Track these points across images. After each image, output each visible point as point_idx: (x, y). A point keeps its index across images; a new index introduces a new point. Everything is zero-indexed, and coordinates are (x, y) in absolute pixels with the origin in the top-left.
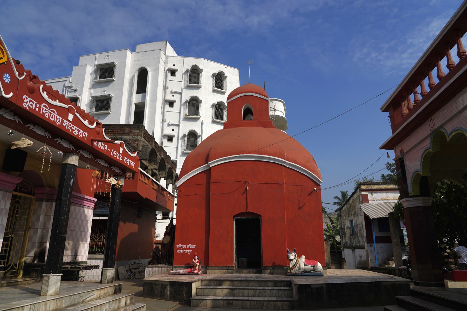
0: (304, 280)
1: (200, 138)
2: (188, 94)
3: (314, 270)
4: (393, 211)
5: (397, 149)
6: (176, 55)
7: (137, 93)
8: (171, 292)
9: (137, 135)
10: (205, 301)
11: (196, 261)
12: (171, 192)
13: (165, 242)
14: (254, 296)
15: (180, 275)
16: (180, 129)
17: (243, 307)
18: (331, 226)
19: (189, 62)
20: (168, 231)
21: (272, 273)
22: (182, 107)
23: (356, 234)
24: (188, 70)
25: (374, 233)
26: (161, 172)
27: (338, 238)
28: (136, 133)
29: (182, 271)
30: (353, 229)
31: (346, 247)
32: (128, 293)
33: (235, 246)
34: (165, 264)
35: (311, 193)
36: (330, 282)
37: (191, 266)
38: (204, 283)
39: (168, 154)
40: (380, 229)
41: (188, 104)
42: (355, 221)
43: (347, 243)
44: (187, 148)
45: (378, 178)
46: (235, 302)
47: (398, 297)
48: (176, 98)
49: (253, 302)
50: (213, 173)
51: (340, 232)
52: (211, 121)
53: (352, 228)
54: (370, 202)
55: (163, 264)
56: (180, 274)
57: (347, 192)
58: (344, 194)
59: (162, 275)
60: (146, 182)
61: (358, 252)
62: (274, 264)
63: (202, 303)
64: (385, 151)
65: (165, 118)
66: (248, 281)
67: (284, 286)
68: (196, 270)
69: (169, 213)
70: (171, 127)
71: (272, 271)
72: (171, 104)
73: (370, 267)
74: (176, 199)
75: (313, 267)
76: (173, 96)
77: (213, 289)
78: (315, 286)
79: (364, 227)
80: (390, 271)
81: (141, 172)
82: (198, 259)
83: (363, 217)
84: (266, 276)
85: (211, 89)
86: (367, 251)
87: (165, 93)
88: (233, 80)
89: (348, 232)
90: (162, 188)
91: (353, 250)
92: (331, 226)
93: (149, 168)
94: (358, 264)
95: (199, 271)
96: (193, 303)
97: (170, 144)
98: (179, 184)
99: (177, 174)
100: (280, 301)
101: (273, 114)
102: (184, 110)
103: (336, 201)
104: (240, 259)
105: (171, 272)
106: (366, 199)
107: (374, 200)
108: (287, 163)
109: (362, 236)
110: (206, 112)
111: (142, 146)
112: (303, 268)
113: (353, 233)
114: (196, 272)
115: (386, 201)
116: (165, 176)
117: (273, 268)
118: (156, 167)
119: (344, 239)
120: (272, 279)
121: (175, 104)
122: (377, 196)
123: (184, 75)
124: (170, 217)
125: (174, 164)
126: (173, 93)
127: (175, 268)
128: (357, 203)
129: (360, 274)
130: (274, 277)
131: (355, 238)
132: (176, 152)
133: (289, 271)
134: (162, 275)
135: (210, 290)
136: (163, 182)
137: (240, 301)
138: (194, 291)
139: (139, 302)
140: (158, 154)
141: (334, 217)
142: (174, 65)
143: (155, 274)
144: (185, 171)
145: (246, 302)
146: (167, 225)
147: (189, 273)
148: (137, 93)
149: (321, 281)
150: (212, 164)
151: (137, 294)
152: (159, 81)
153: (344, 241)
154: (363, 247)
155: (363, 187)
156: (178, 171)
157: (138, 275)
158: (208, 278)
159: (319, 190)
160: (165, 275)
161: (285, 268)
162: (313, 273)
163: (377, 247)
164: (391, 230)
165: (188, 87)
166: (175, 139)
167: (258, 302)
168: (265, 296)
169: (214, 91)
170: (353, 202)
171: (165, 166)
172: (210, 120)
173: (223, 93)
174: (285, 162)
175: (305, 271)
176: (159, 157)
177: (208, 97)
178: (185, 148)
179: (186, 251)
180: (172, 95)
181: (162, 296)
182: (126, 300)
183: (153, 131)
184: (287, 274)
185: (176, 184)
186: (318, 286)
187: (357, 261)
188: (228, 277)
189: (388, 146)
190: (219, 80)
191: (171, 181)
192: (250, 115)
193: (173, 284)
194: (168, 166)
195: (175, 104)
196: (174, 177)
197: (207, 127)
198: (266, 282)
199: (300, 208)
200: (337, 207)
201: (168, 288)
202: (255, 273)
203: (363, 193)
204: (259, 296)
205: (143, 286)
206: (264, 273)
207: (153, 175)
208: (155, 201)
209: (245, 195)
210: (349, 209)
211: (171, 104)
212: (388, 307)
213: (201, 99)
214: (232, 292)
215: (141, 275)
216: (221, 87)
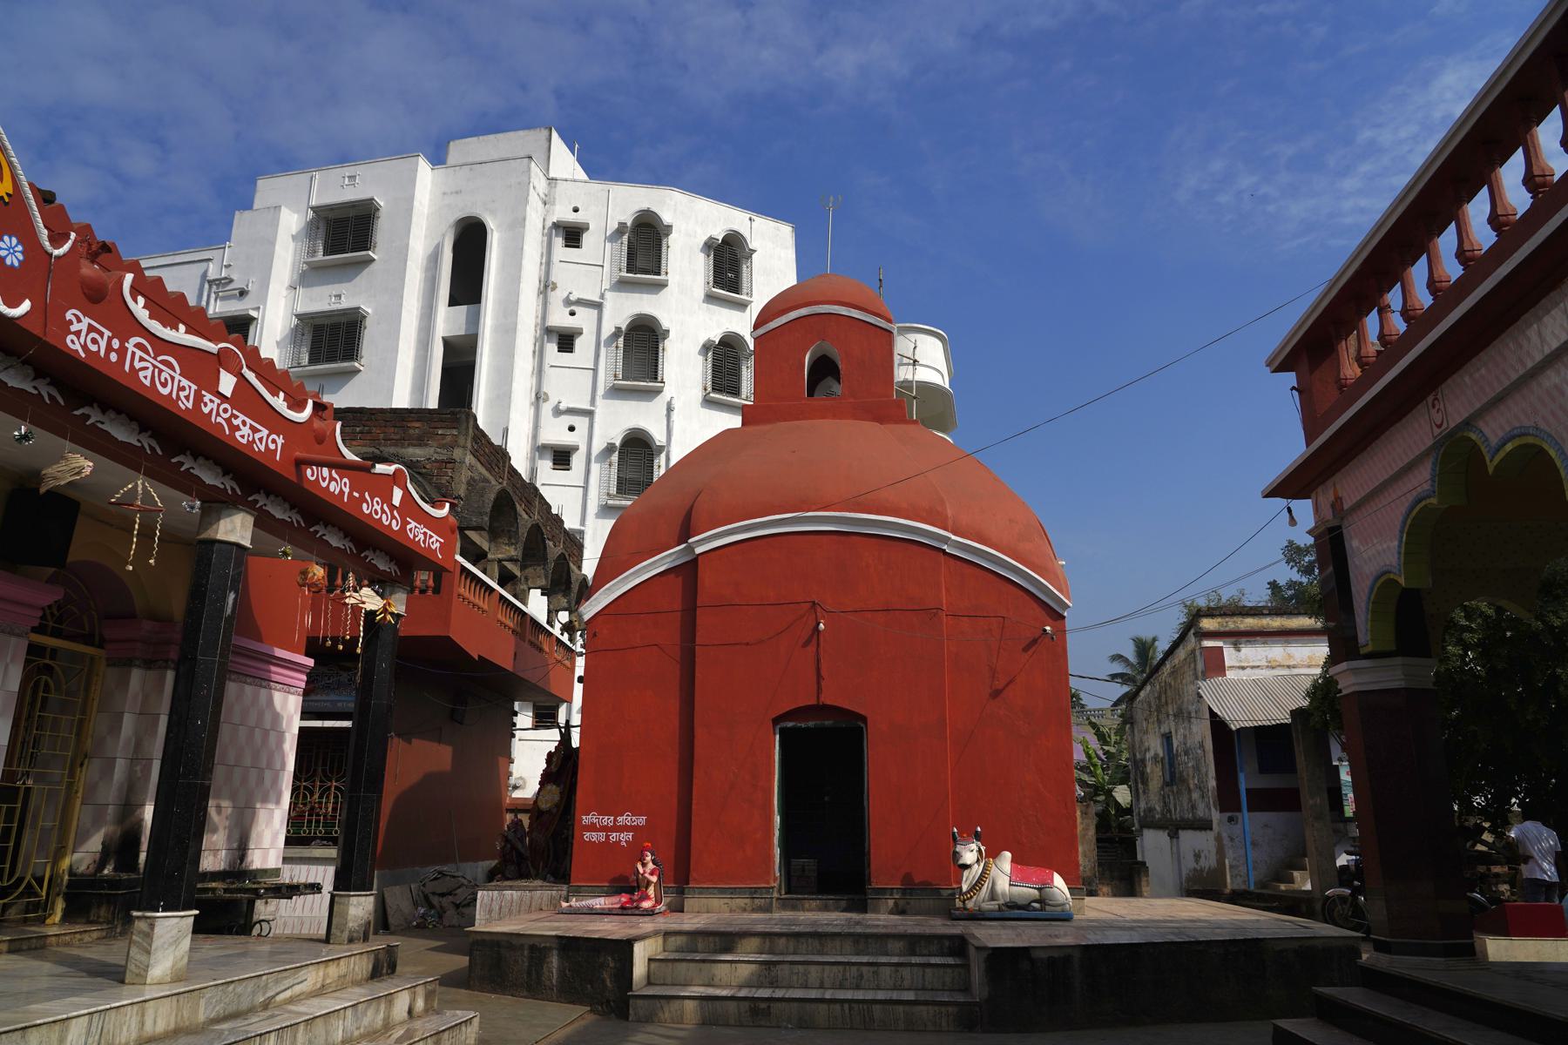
0: (1009, 932)
1: (663, 456)
2: (622, 310)
4: (1305, 703)
5: (1321, 499)
10: (676, 1004)
11: (647, 868)
13: (544, 806)
14: (841, 987)
15: (592, 915)
17: (804, 1024)
18: (1100, 753)
19: (627, 200)
21: (901, 911)
22: (603, 350)
23: (1184, 781)
24: (622, 225)
25: (1242, 777)
26: (530, 571)
27: (1122, 794)
28: (449, 439)
29: (599, 903)
30: (1172, 765)
31: (1150, 823)
33: (777, 819)
34: (544, 879)
35: (1035, 641)
36: (1094, 939)
37: (629, 886)
38: (675, 941)
39: (554, 511)
40: (1258, 761)
41: (621, 340)
43: (1151, 810)
44: (619, 490)
45: (1258, 595)
46: (776, 1007)
48: (584, 320)
49: (838, 1007)
50: (706, 577)
51: (1128, 773)
53: (1170, 759)
54: (1230, 674)
55: (536, 877)
56: (591, 912)
57: (1154, 640)
58: (1143, 648)
59: (534, 917)
61: (1190, 840)
62: (907, 878)
63: (666, 1009)
64: (1280, 502)
65: (545, 389)
66: (820, 937)
67: (942, 955)
69: (556, 708)
71: (901, 903)
72: (566, 341)
74: (580, 663)
75: (1040, 889)
76: (572, 314)
77: (704, 961)
78: (1043, 955)
80: (1293, 905)
81: (463, 569)
82: (654, 862)
84: (881, 919)
86: (1219, 839)
88: (775, 262)
89: (1155, 774)
90: (535, 623)
91: (1174, 836)
92: (1100, 753)
93: (490, 556)
95: (658, 902)
96: (637, 1008)
97: (561, 476)
98: (590, 609)
99: (585, 578)
100: (926, 1003)
101: (910, 377)
102: (611, 363)
103: (1118, 668)
104: (794, 861)
105: (565, 905)
106: (1216, 665)
107: (1243, 668)
108: (954, 542)
109: (1201, 788)
110: (683, 368)
111: (468, 483)
112: (1004, 894)
113: (1174, 779)
114: (646, 904)
115: (1285, 672)
116: (543, 582)
120: (901, 930)
121: (579, 343)
122: (1253, 653)
123: (608, 245)
124: (562, 720)
125: (574, 543)
126: (573, 304)
127: (577, 892)
128: (1189, 677)
131: (1179, 792)
132: (580, 503)
133: (959, 904)
134: (534, 917)
136: (537, 605)
138: (639, 969)
139: (455, 1004)
141: (1110, 723)
142: (576, 210)
144: (610, 566)
145: (814, 1006)
146: (552, 747)
147: (622, 908)
149: (1064, 937)
150: (704, 542)
151: (450, 981)
153: (1143, 805)
154: (1205, 825)
155: (1207, 624)
156: (589, 568)
157: (451, 916)
158: (687, 927)
159: (1061, 632)
160: (543, 915)
161: (945, 893)
162: (1039, 911)
163: (1251, 822)
165: (622, 285)
166: (577, 461)
168: (878, 988)
169: (710, 298)
170: (1174, 672)
171: (544, 550)
172: (697, 394)
173: (742, 306)
174: (946, 540)
175: (1012, 905)
176: (525, 519)
177: (691, 318)
178: (613, 490)
179: (614, 836)
181: (533, 987)
183: (506, 431)
184: (951, 915)
185: (581, 609)
186: (1056, 954)
188: (755, 922)
189: (1290, 486)
190: (728, 261)
192: (830, 381)
193: (569, 945)
194: (554, 550)
195: (578, 343)
196: (575, 587)
197: (687, 419)
198: (879, 940)
199: (996, 694)
200: (1120, 690)
201: (554, 961)
203: (1208, 643)
204: (858, 988)
205: (470, 953)
206: (876, 911)
207: (506, 579)
209: (811, 649)
210: (1159, 698)
211: (566, 341)
213: (665, 324)
214: (768, 972)
215: (462, 915)
216: (735, 286)
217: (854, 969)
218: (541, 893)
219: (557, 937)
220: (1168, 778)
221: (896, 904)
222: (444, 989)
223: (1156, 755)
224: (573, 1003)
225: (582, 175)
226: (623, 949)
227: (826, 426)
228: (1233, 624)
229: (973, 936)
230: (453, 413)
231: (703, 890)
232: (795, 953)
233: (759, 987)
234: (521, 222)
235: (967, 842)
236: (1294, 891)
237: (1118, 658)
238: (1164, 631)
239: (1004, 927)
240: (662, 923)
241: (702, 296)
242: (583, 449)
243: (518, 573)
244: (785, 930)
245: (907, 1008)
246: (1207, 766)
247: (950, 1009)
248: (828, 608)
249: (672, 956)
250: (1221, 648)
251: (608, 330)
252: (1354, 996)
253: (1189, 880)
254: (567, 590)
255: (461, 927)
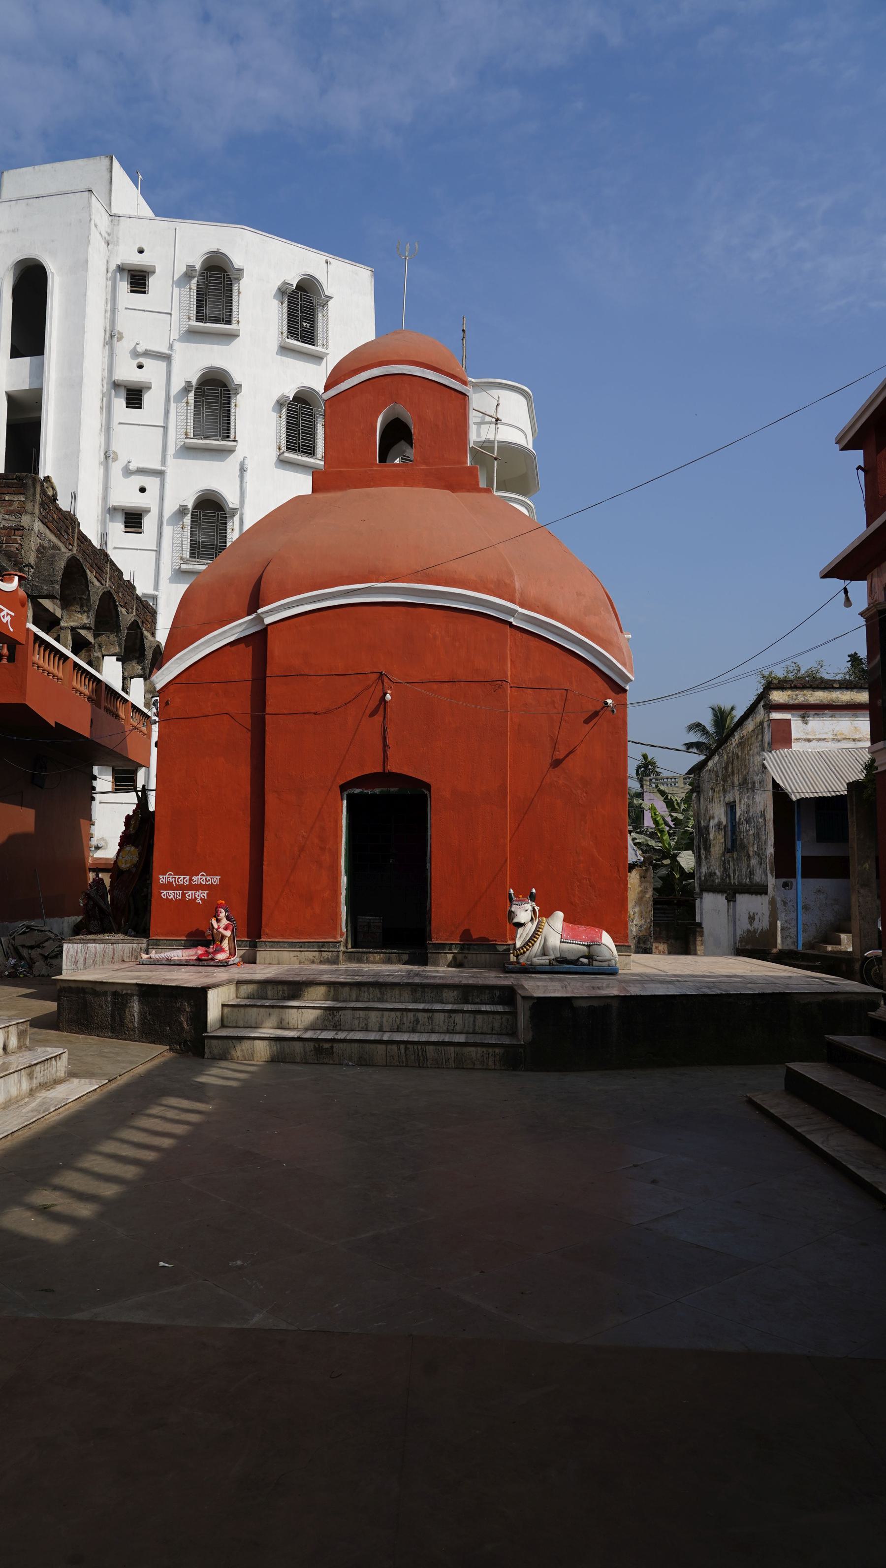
0: (556, 984)
1: (236, 518)
2: (194, 361)
3: (590, 957)
4: (861, 776)
5: (875, 580)
6: (147, 212)
7: (12, 357)
8: (140, 1013)
9: (20, 512)
10: (246, 1044)
11: (221, 924)
12: (141, 706)
13: (123, 866)
14: (399, 1030)
15: (171, 966)
16: (167, 486)
17: (364, 1062)
18: (669, 819)
19: (196, 240)
21: (457, 963)
22: (173, 406)
23: (744, 848)
24: (190, 270)
25: (799, 845)
26: (103, 638)
27: (687, 860)
28: (16, 505)
29: (178, 955)
30: (734, 832)
31: (710, 887)
32: (10, 1018)
33: (344, 879)
34: (126, 934)
35: (596, 714)
36: (635, 991)
37: (202, 939)
38: (246, 989)
39: (126, 577)
40: (818, 831)
41: (191, 395)
42: (743, 807)
43: (711, 875)
44: (192, 554)
46: (338, 1047)
47: (831, 1037)
48: (152, 374)
49: (395, 1047)
51: (692, 839)
52: (274, 459)
53: (733, 828)
54: (795, 746)
55: (117, 932)
56: (170, 963)
57: (732, 709)
58: (720, 716)
59: (116, 967)
60: (55, 672)
61: (746, 903)
62: (466, 935)
63: (238, 1048)
64: (837, 584)
65: (114, 447)
66: (380, 987)
68: (223, 950)
69: (135, 772)
71: (459, 957)
72: (134, 397)
73: (775, 951)
74: (155, 728)
75: (588, 946)
76: (140, 367)
77: (272, 1007)
78: (584, 1004)
79: (771, 825)
81: (37, 637)
82: (228, 918)
83: (770, 795)
84: (440, 971)
86: (772, 902)
87: (111, 355)
88: (352, 317)
89: (717, 840)
90: (110, 690)
91: (731, 899)
92: (669, 819)
93: (63, 624)
95: (232, 954)
96: (212, 1047)
97: (133, 539)
98: (163, 677)
99: (158, 646)
100: (475, 1045)
101: (492, 438)
102: (182, 417)
103: (694, 737)
104: (361, 919)
105: (145, 956)
107: (809, 740)
108: (521, 615)
109: (760, 855)
110: (257, 424)
111: (38, 550)
112: (554, 949)
113: (735, 845)
114: (221, 956)
115: (851, 745)
116: (117, 650)
117: (462, 947)
118: (85, 619)
119: (704, 863)
120: (456, 981)
122: (819, 726)
123: (176, 290)
124: (139, 786)
125: (147, 610)
126: (141, 356)
127: (156, 944)
128: (755, 750)
129: (733, 972)
131: (739, 858)
132: (153, 568)
133: (513, 958)
134: (116, 967)
135: (262, 1010)
136: (111, 671)
137: (356, 1045)
138: (213, 1013)
139: (45, 1043)
140: (91, 576)
141: (679, 793)
142: (141, 251)
144: (182, 636)
145: (373, 1046)
146: (130, 810)
147: (199, 959)
148: (12, 357)
149: (611, 989)
150: (272, 613)
151: (39, 1023)
153: (704, 870)
154: (761, 890)
155: (777, 696)
156: (162, 636)
157: (40, 967)
159: (622, 705)
160: (125, 965)
161: (501, 949)
162: (586, 964)
163: (803, 887)
164: (851, 836)
165: (192, 335)
166: (149, 523)
168: (433, 1032)
169: (284, 350)
170: (742, 744)
171: (118, 619)
172: (272, 454)
173: (318, 358)
174: (513, 612)
175: (562, 960)
176: (97, 586)
177: (265, 372)
178: (187, 554)
179: (190, 894)
180: (135, 363)
181: (117, 1028)
182: (7, 1038)
183: (74, 496)
184: (505, 968)
185: (154, 678)
186: (595, 1003)
188: (322, 972)
190: (302, 308)
191: (138, 669)
192: (403, 445)
193: (147, 992)
194: (127, 617)
195: (147, 398)
196: (149, 654)
198: (437, 989)
199: (556, 763)
200: (696, 758)
203: (776, 715)
204: (414, 1031)
205: (57, 999)
206: (436, 964)
207: (79, 646)
208: (87, 734)
209: (378, 718)
210: (726, 768)
211: (134, 397)
212: (794, 1066)
213: (237, 378)
214: (331, 1017)
215: (51, 965)
216: (309, 337)
217: (411, 1015)
218: (123, 946)
219: (137, 984)
220: (729, 845)
221: (454, 958)
222: (35, 1030)
223: (720, 823)
226: (199, 995)
227: (398, 493)
228: (803, 696)
229: (523, 987)
230: (19, 479)
231: (274, 944)
232: (357, 1001)
233: (322, 1030)
234: (82, 265)
235: (521, 902)
236: (841, 952)
237: (697, 727)
238: (739, 699)
239: (551, 980)
240: (236, 973)
241: (275, 347)
242: (155, 511)
243: (91, 639)
245: (458, 1049)
247: (497, 1051)
248: (396, 679)
249: (248, 1002)
250: (788, 721)
251: (177, 385)
252: (861, 1044)
253: (742, 940)
255: (49, 976)
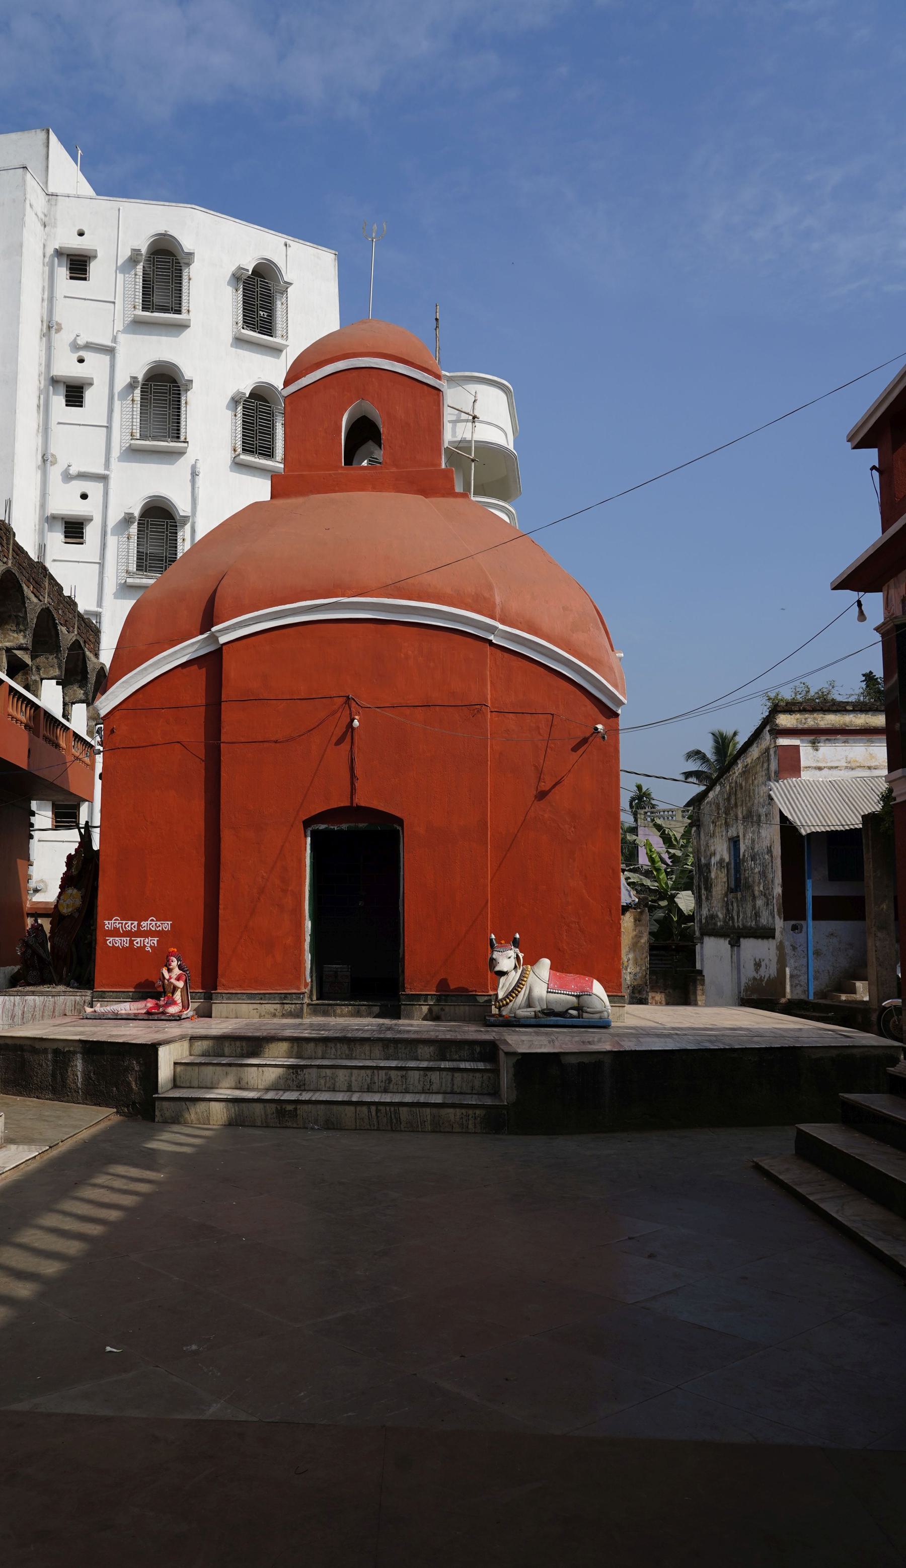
1: (188, 527)
2: (139, 355)
3: (579, 1008)
5: (892, 592)
10: (202, 1106)
11: (173, 974)
13: (65, 911)
14: (369, 1090)
15: (118, 1021)
17: (330, 1125)
18: (666, 856)
20: (74, 871)
21: (432, 1016)
22: (117, 404)
23: (749, 887)
24: (136, 252)
25: (809, 884)
26: (41, 660)
27: (686, 901)
29: (125, 1008)
33: (308, 924)
35: (585, 741)
36: (629, 1045)
37: (152, 990)
38: (200, 1046)
39: (66, 593)
41: (138, 392)
42: (748, 842)
43: (712, 917)
44: (140, 567)
45: (850, 688)
46: (302, 1109)
48: (94, 368)
49: (365, 1109)
50: (231, 667)
53: (736, 865)
54: (805, 775)
55: (58, 983)
57: (735, 734)
58: (722, 742)
61: (751, 948)
62: (443, 985)
63: (192, 1111)
64: (851, 596)
65: (52, 450)
66: (349, 1042)
67: (473, 1060)
68: (174, 1003)
69: (77, 807)
70: (74, 482)
71: (435, 1009)
72: (75, 394)
73: (783, 1000)
74: (99, 759)
75: (578, 997)
76: (81, 361)
77: (230, 1065)
78: (573, 1060)
80: (850, 1016)
82: (180, 967)
83: (777, 828)
84: (415, 1024)
85: (228, 336)
86: (781, 948)
87: (49, 348)
88: (313, 306)
89: (719, 879)
90: (49, 716)
91: (735, 944)
92: (666, 856)
94: (746, 990)
95: (185, 1007)
96: (167, 1109)
97: (73, 550)
98: (107, 703)
99: (102, 668)
100: (453, 1106)
101: (468, 437)
102: (127, 416)
103: (694, 766)
105: (89, 1010)
106: (790, 764)
107: (820, 769)
108: (501, 632)
109: (766, 895)
110: (210, 424)
112: (540, 1000)
113: (739, 884)
114: (172, 1010)
115: (866, 773)
116: (57, 672)
117: (439, 999)
118: (21, 639)
119: (704, 904)
120: (432, 1035)
121: (89, 395)
122: (832, 753)
123: (120, 276)
124: (82, 823)
125: (90, 629)
126: (82, 350)
127: (102, 997)
128: (760, 779)
129: (738, 1024)
130: (443, 1030)
131: (744, 899)
132: (96, 582)
133: (495, 1011)
134: (58, 1022)
135: (218, 1069)
136: (51, 696)
137: (322, 1107)
138: (165, 1072)
140: (27, 591)
141: (677, 829)
142: (81, 234)
143: (33, 1017)
144: (128, 657)
145: (340, 1108)
146: (72, 849)
147: (148, 1013)
149: (603, 1043)
150: (228, 632)
152: (24, 299)
153: (705, 912)
154: (767, 933)
156: (106, 657)
158: (215, 1032)
159: (614, 731)
160: (67, 1020)
161: (481, 1000)
163: (814, 930)
166: (91, 532)
167: (382, 1108)
168: (407, 1091)
170: (745, 773)
171: (59, 638)
172: (226, 457)
173: (276, 351)
174: (492, 630)
175: (549, 1012)
176: (34, 602)
177: (220, 367)
178: (133, 567)
179: (138, 941)
180: (75, 357)
181: (58, 1089)
183: (9, 504)
184: (486, 1021)
185: (97, 703)
186: (586, 1060)
187: (744, 981)
188: (284, 1027)
189: (859, 579)
190: (259, 294)
191: (80, 693)
192: (371, 445)
194: (67, 636)
195: (88, 395)
196: (92, 677)
197: (216, 485)
198: (411, 1045)
199: (542, 795)
200: (695, 789)
201: (79, 1064)
202: (378, 1016)
203: (783, 741)
204: (386, 1091)
206: (410, 1017)
208: (24, 766)
209: (346, 746)
210: (729, 799)
212: (804, 1127)
214: (294, 1076)
216: (267, 327)
217: (382, 1073)
218: (65, 999)
219: (80, 1041)
220: (733, 885)
221: (430, 1010)
224: (99, 1105)
225: (88, 190)
233: (287, 1089)
236: (856, 1002)
237: (697, 754)
239: (537, 1034)
241: (230, 339)
243: (28, 661)
244: (314, 1035)
245: (435, 1110)
246: (774, 872)
247: (478, 1112)
250: (797, 748)
251: (122, 381)
252: (879, 1102)
254: (83, 680)
